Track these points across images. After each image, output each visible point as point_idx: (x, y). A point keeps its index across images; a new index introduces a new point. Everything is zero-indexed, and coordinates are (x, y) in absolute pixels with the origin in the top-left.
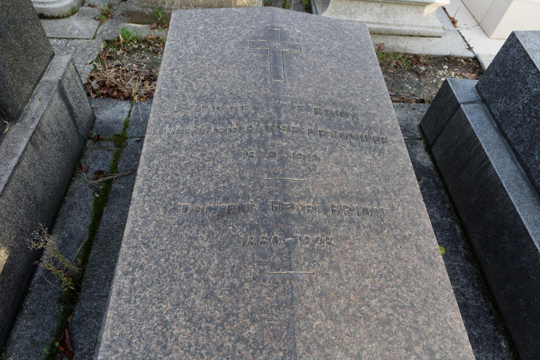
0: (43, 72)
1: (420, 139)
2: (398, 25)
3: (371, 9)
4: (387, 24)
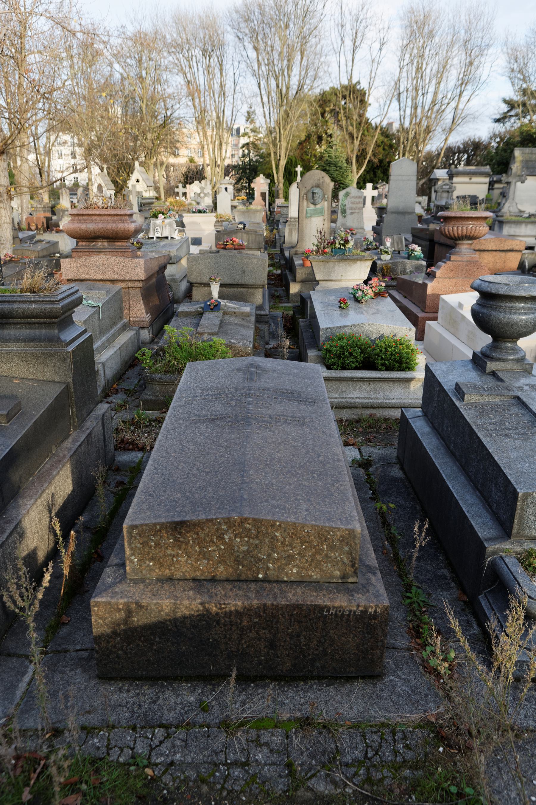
0: (92, 410)
1: (397, 464)
2: (389, 399)
3: (360, 387)
4: (377, 399)
